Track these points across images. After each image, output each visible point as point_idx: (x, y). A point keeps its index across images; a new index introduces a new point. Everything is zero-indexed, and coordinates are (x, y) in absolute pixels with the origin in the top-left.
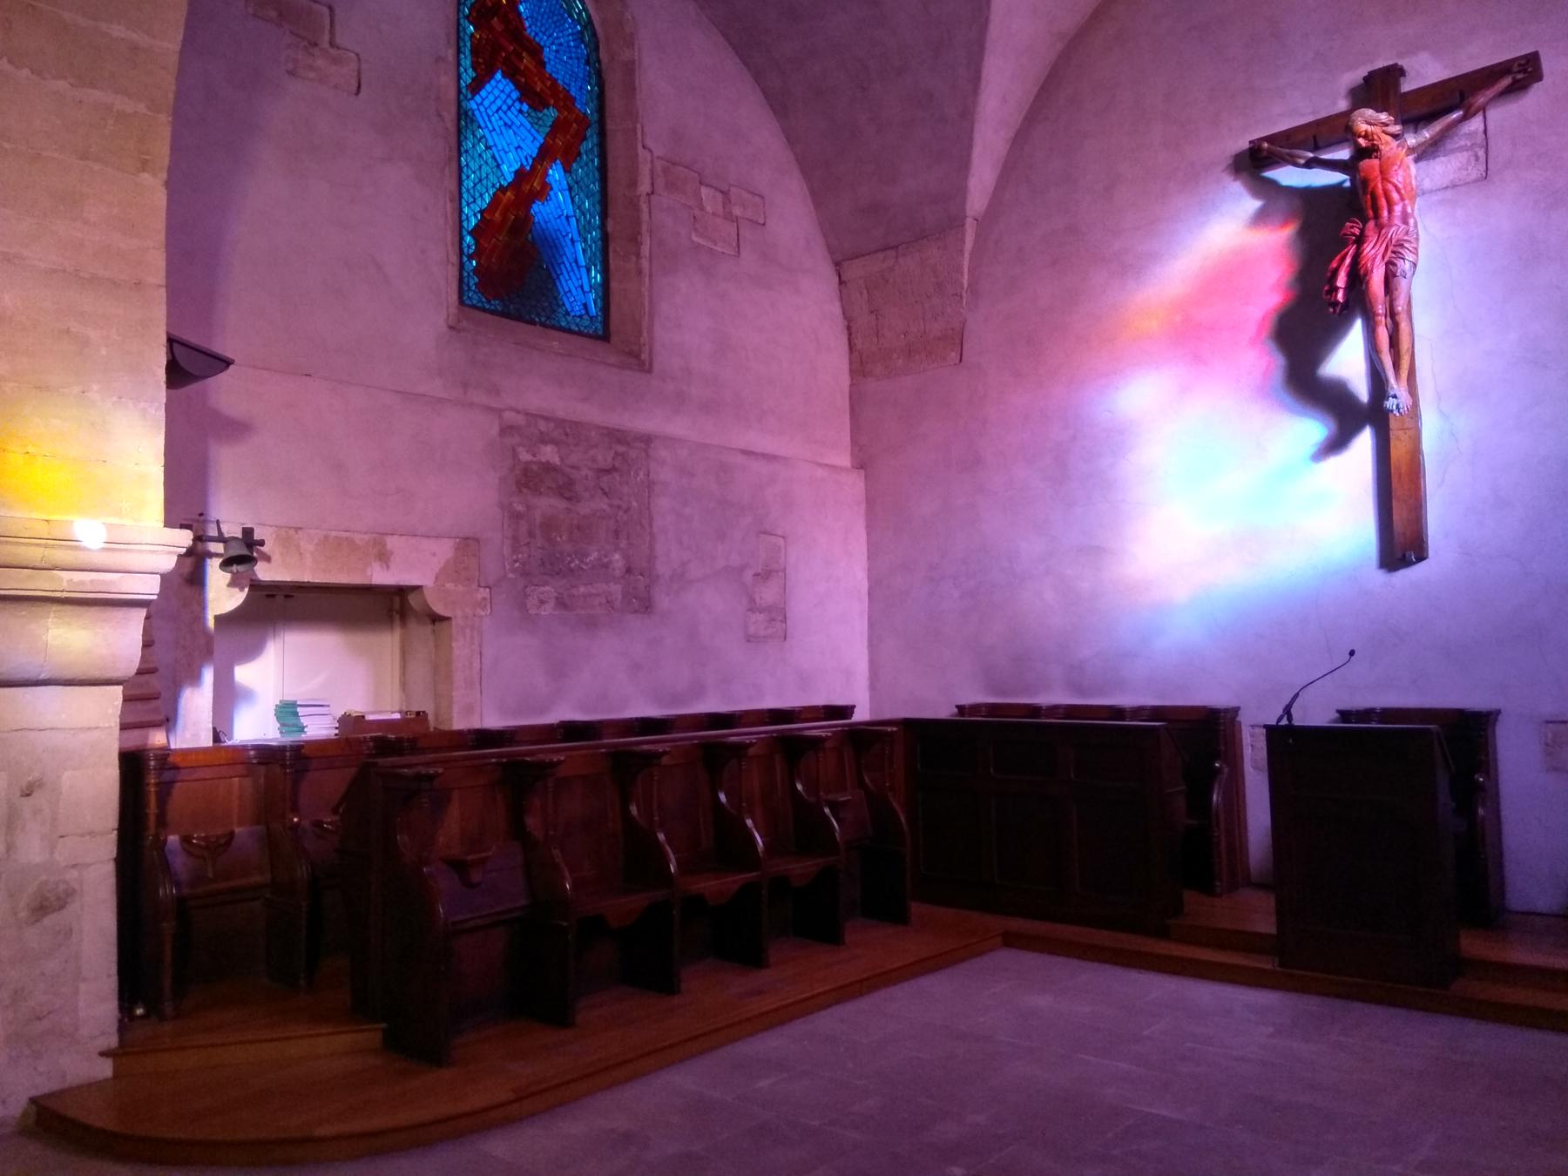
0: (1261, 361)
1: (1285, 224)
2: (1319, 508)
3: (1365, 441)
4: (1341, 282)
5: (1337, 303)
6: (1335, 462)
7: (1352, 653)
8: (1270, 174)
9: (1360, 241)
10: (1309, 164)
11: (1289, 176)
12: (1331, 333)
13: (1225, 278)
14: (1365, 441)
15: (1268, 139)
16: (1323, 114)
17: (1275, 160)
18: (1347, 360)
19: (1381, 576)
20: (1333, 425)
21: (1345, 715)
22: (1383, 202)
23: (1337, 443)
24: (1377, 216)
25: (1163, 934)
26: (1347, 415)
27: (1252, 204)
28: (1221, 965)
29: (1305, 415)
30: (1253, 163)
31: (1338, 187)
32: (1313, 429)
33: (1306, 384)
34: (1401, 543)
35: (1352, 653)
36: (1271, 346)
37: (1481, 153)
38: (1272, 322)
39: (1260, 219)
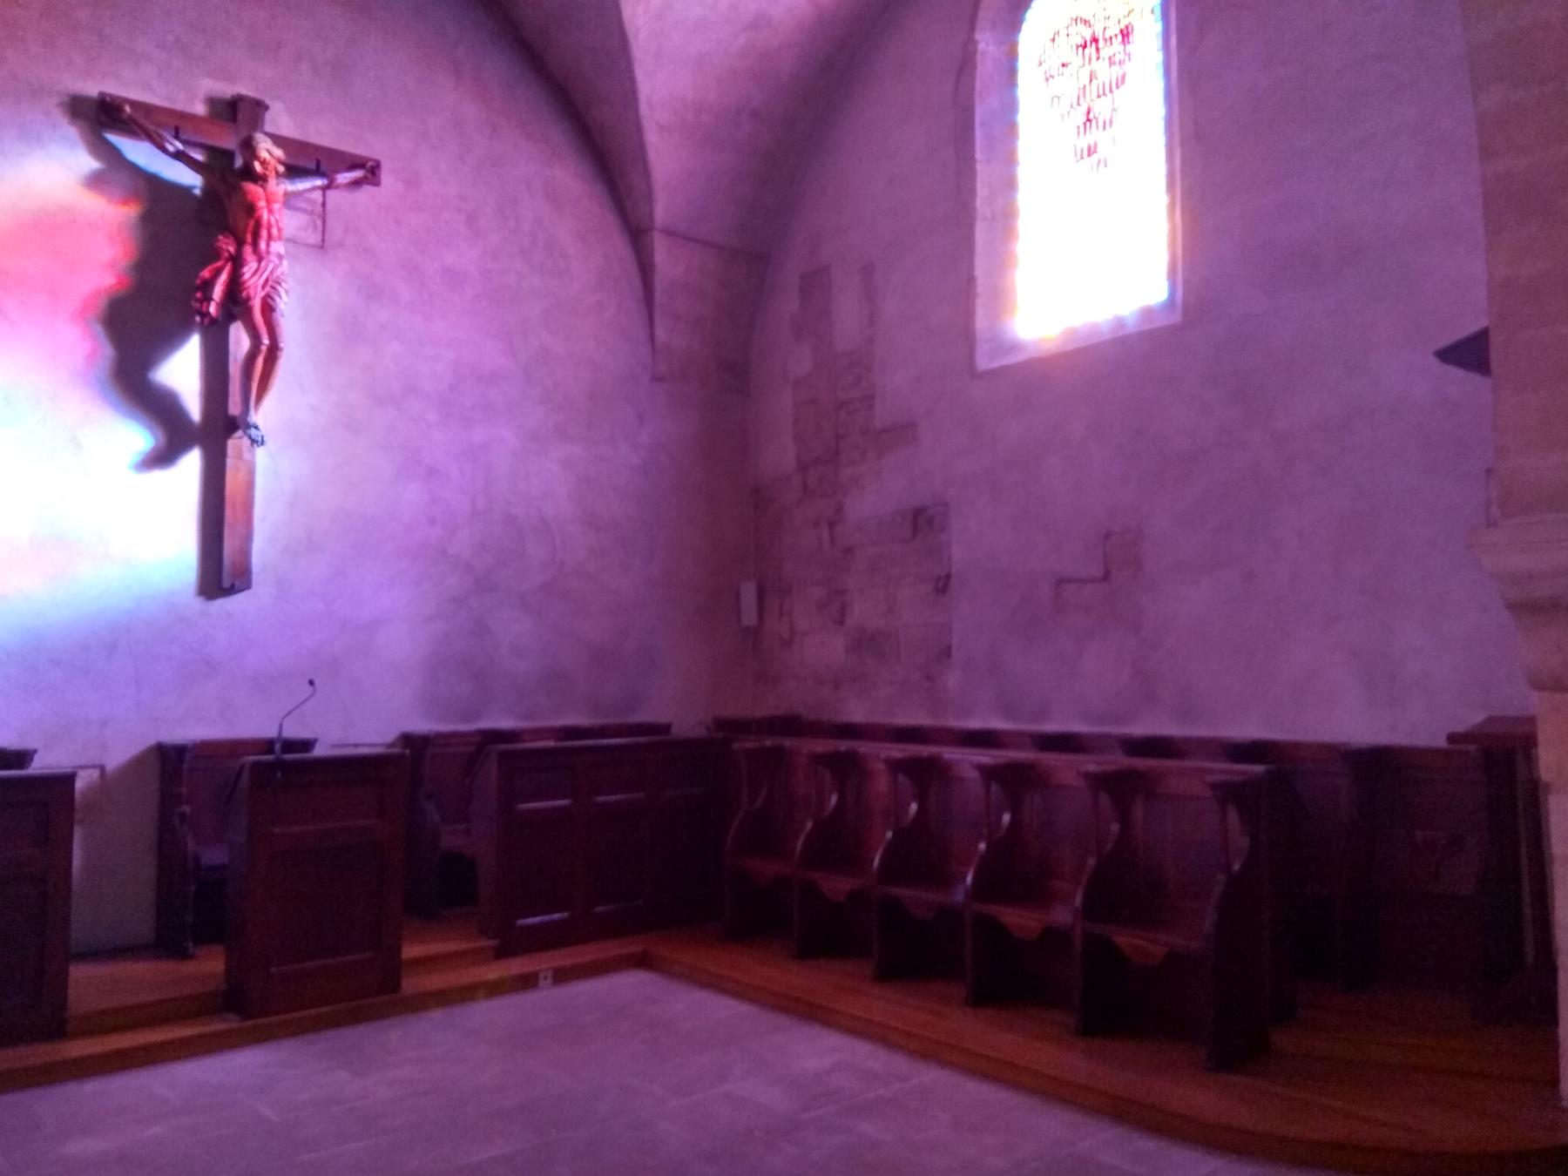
0: (82, 345)
1: (125, 202)
2: (128, 525)
3: (192, 463)
4: (218, 291)
5: (208, 314)
6: (159, 475)
7: (311, 683)
8: (114, 138)
9: (237, 262)
10: (179, 156)
11: (139, 153)
12: (169, 340)
13: (46, 229)
14: (192, 463)
15: (133, 104)
16: (178, 107)
17: (132, 128)
18: (182, 371)
19: (198, 603)
20: (162, 438)
21: (1452, 738)
22: (264, 233)
23: (162, 457)
24: (255, 244)
25: (58, 1030)
26: (173, 433)
27: (86, 162)
28: (171, 1043)
29: (130, 415)
30: (102, 117)
31: (185, 191)
32: (139, 437)
33: (133, 385)
34: (220, 571)
35: (311, 683)
36: (99, 330)
37: (319, 222)
38: (102, 303)
39: (95, 182)
